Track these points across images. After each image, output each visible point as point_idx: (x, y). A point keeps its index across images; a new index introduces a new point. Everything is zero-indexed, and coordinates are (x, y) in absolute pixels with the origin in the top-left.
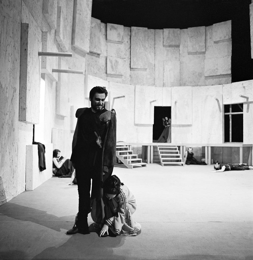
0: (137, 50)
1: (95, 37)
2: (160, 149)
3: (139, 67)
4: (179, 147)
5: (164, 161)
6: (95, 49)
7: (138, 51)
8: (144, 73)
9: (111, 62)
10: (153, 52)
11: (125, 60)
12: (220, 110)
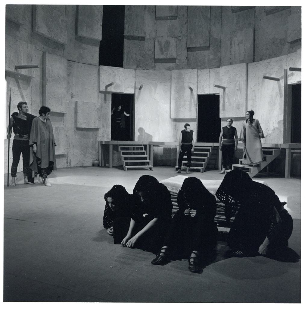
0: (195, 23)
1: (137, 17)
2: (122, 149)
3: (198, 46)
4: (145, 146)
5: (127, 164)
6: (137, 32)
7: (197, 24)
8: (206, 53)
9: (160, 43)
10: (219, 23)
11: (180, 38)
12: (281, 94)
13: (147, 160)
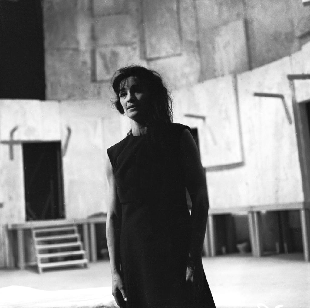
9: (103, 57)
13: (104, 224)
